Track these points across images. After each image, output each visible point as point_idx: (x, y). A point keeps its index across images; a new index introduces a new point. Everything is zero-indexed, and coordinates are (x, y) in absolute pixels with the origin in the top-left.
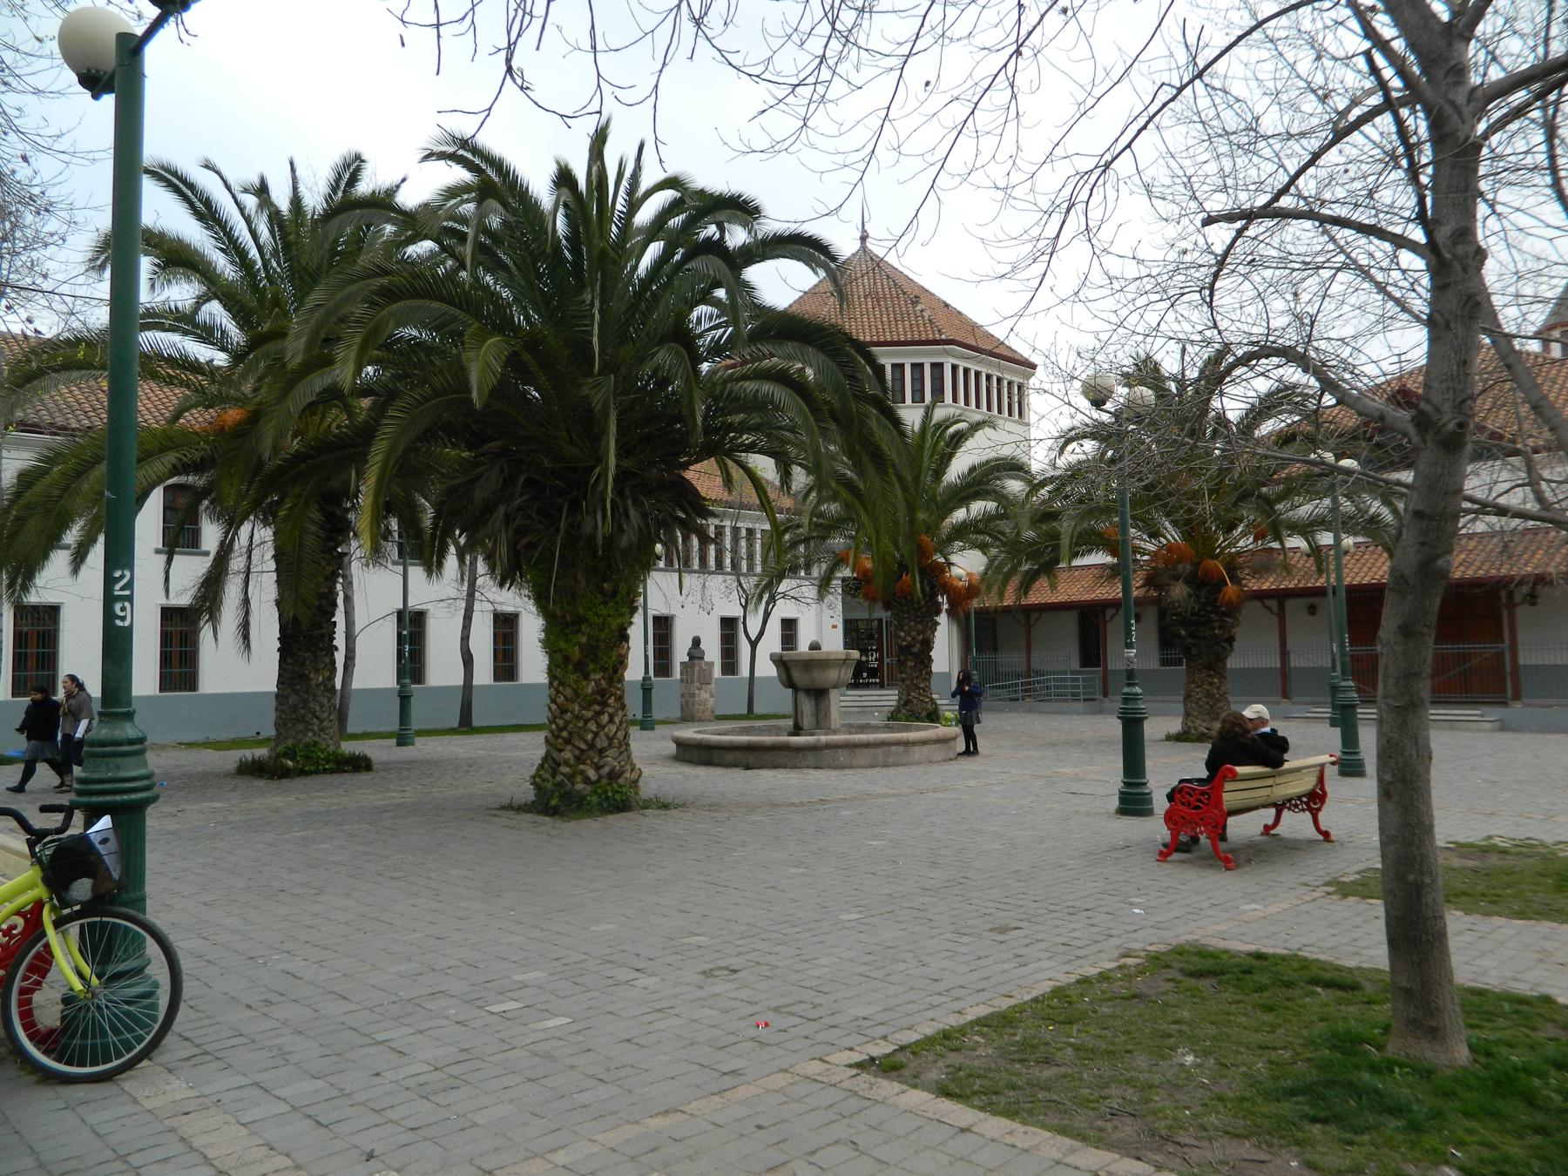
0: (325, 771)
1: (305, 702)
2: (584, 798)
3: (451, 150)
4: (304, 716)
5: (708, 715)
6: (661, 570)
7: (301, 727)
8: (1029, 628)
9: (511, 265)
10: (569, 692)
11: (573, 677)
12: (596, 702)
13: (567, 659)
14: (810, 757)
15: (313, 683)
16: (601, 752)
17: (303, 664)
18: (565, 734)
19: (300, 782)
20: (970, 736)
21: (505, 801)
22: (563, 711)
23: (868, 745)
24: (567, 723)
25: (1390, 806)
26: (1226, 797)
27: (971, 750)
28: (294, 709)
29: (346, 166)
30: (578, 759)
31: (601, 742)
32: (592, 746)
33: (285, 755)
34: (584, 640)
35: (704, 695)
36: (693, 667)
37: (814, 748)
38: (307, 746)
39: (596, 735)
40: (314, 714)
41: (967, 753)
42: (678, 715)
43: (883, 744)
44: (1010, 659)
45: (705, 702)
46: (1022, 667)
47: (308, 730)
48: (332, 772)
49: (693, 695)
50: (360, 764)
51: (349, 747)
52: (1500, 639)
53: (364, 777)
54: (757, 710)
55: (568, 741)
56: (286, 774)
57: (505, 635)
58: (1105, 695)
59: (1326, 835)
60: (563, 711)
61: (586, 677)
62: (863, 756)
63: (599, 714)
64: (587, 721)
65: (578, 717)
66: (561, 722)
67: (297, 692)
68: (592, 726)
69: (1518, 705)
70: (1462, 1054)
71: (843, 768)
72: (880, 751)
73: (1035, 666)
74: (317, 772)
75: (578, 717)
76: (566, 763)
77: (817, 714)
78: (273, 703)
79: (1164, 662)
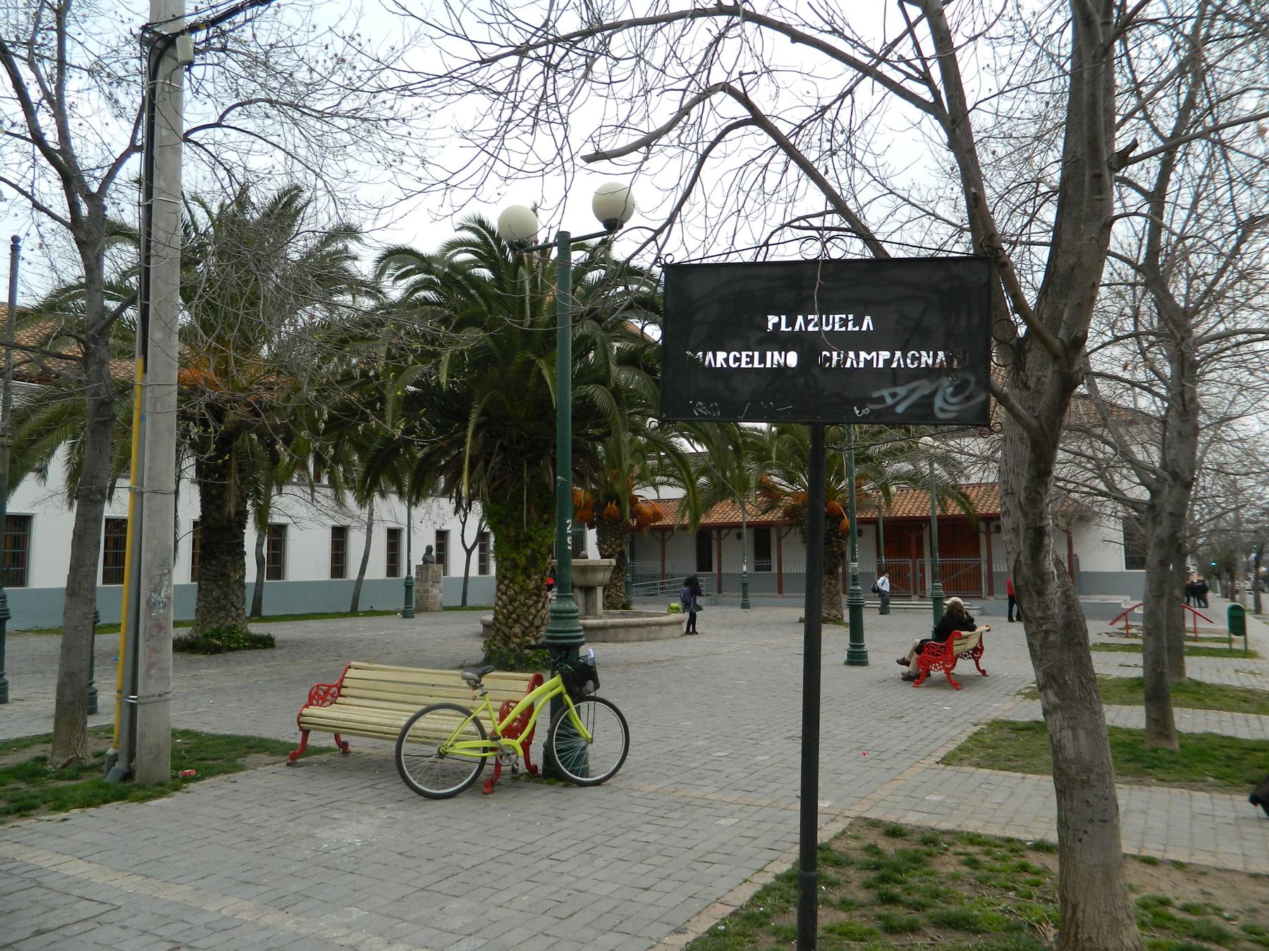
0: (245, 648)
1: (226, 595)
2: (529, 659)
3: (473, 225)
4: (225, 606)
5: (437, 607)
6: (294, 484)
7: (222, 614)
8: (663, 542)
9: (477, 295)
10: (517, 587)
11: (522, 577)
12: (534, 594)
13: (515, 566)
14: (600, 633)
15: (232, 580)
16: (537, 628)
17: (225, 565)
18: (514, 616)
19: (230, 655)
20: (692, 620)
21: (459, 663)
22: (512, 600)
23: (638, 626)
24: (515, 609)
25: (1150, 639)
26: (955, 648)
27: (691, 629)
28: (217, 600)
29: (285, 193)
30: (524, 634)
31: (537, 622)
32: (531, 624)
33: (212, 636)
34: (529, 552)
35: (435, 591)
36: (427, 569)
37: (603, 628)
38: (229, 628)
39: (535, 616)
40: (232, 604)
41: (688, 632)
42: (349, 610)
43: (648, 625)
44: (648, 565)
45: (435, 597)
46: (659, 570)
47: (228, 616)
48: (250, 648)
49: (427, 591)
50: (266, 643)
51: (256, 629)
52: (978, 554)
53: (266, 653)
54: (469, 602)
55: (516, 621)
56: (217, 650)
57: (116, 539)
58: (720, 591)
59: (983, 672)
60: (512, 600)
61: (529, 577)
62: (634, 634)
63: (537, 602)
64: (529, 608)
65: (524, 605)
66: (511, 608)
67: (220, 587)
68: (533, 611)
69: (992, 598)
70: (1177, 746)
71: (623, 642)
72: (644, 630)
73: (668, 571)
74: (238, 649)
75: (524, 605)
76: (516, 635)
77: (586, 605)
78: (62, 600)
79: (757, 569)
